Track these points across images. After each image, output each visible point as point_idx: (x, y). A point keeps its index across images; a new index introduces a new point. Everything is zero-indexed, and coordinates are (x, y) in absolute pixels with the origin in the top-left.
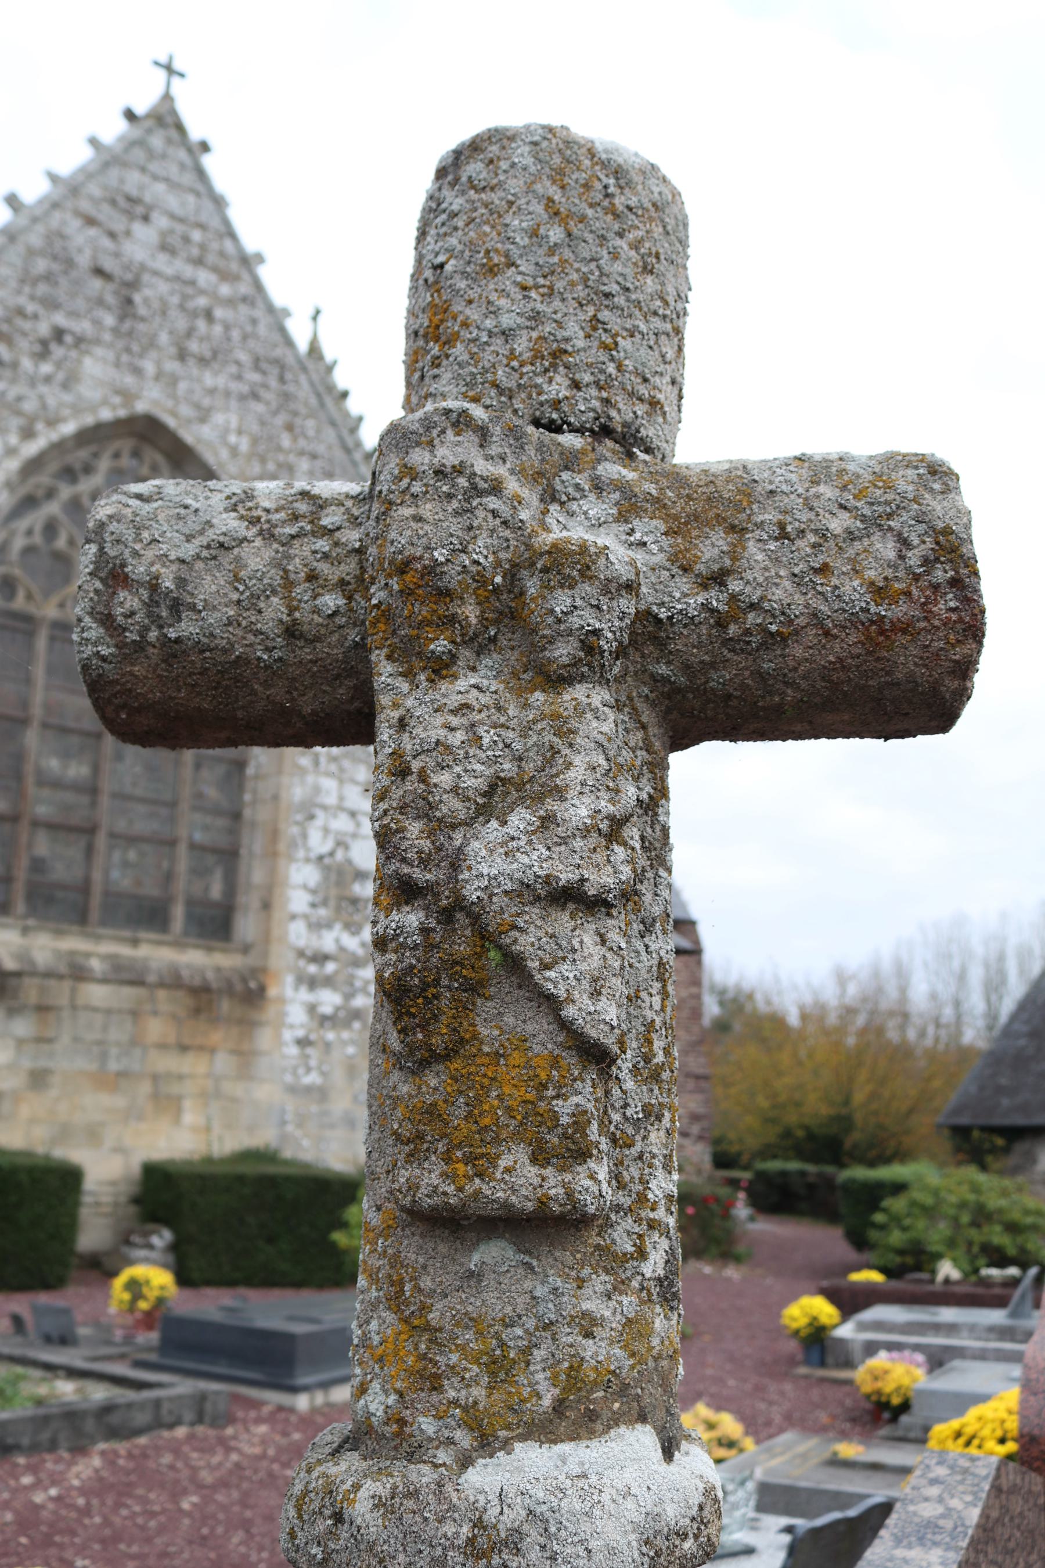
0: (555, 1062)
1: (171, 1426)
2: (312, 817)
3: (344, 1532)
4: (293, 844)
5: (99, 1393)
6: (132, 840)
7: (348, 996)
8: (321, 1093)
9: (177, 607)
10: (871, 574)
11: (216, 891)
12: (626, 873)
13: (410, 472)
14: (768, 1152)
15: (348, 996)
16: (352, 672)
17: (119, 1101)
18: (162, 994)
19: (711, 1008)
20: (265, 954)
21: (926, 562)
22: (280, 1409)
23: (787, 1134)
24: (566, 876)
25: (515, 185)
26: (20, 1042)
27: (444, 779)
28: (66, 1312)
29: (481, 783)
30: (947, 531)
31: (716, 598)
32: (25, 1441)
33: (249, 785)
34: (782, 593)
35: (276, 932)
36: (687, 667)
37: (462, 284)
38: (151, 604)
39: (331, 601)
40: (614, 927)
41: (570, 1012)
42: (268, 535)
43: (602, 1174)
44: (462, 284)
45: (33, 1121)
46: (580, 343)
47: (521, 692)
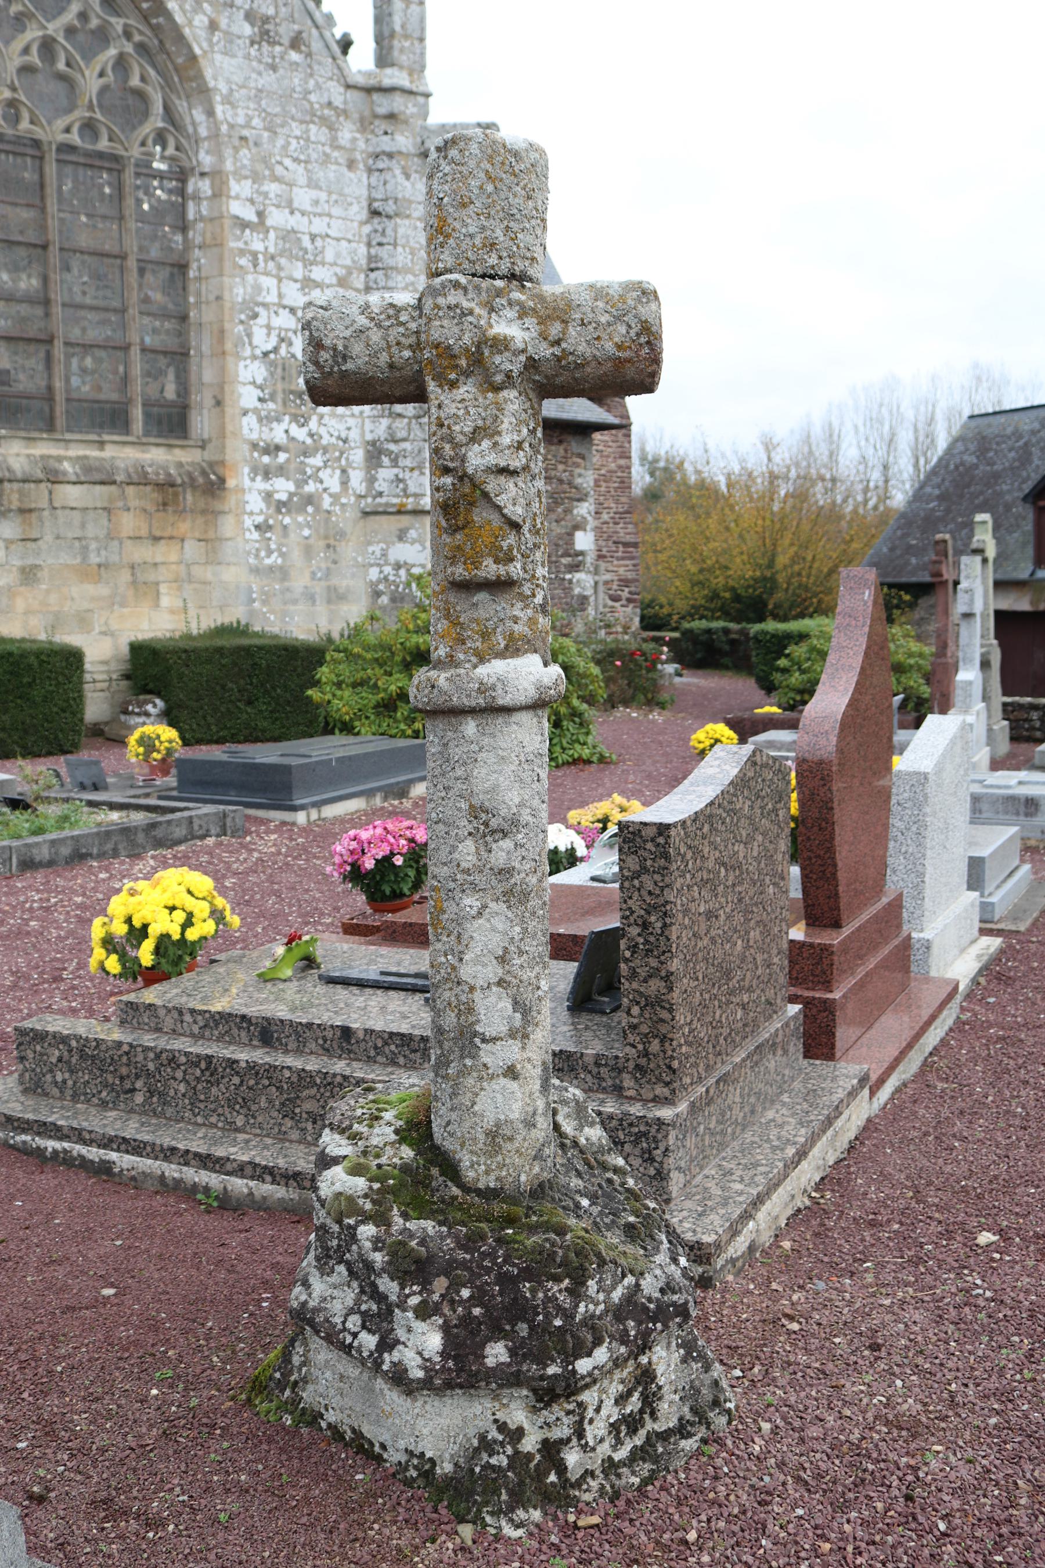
0: (501, 529)
1: (203, 837)
2: (255, 316)
3: (435, 691)
4: (239, 343)
5: (138, 818)
6: (88, 348)
7: (300, 484)
8: (282, 573)
9: (345, 357)
10: (616, 340)
11: (170, 392)
12: (524, 460)
13: (437, 307)
14: (694, 613)
15: (300, 484)
16: (415, 381)
17: (103, 590)
18: (130, 490)
19: (640, 478)
20: (223, 448)
21: (638, 335)
22: (284, 823)
23: (715, 596)
24: (503, 464)
25: (472, 164)
26: (8, 543)
27: (457, 428)
28: (97, 763)
29: (471, 429)
30: (646, 321)
31: (557, 350)
32: (95, 851)
33: (192, 287)
34: (582, 348)
35: (229, 428)
36: (546, 377)
37: (451, 210)
38: (334, 356)
39: (407, 354)
40: (520, 481)
41: (505, 511)
42: (379, 326)
43: (519, 566)
44: (451, 210)
45: (27, 612)
46: (501, 239)
47: (484, 392)
